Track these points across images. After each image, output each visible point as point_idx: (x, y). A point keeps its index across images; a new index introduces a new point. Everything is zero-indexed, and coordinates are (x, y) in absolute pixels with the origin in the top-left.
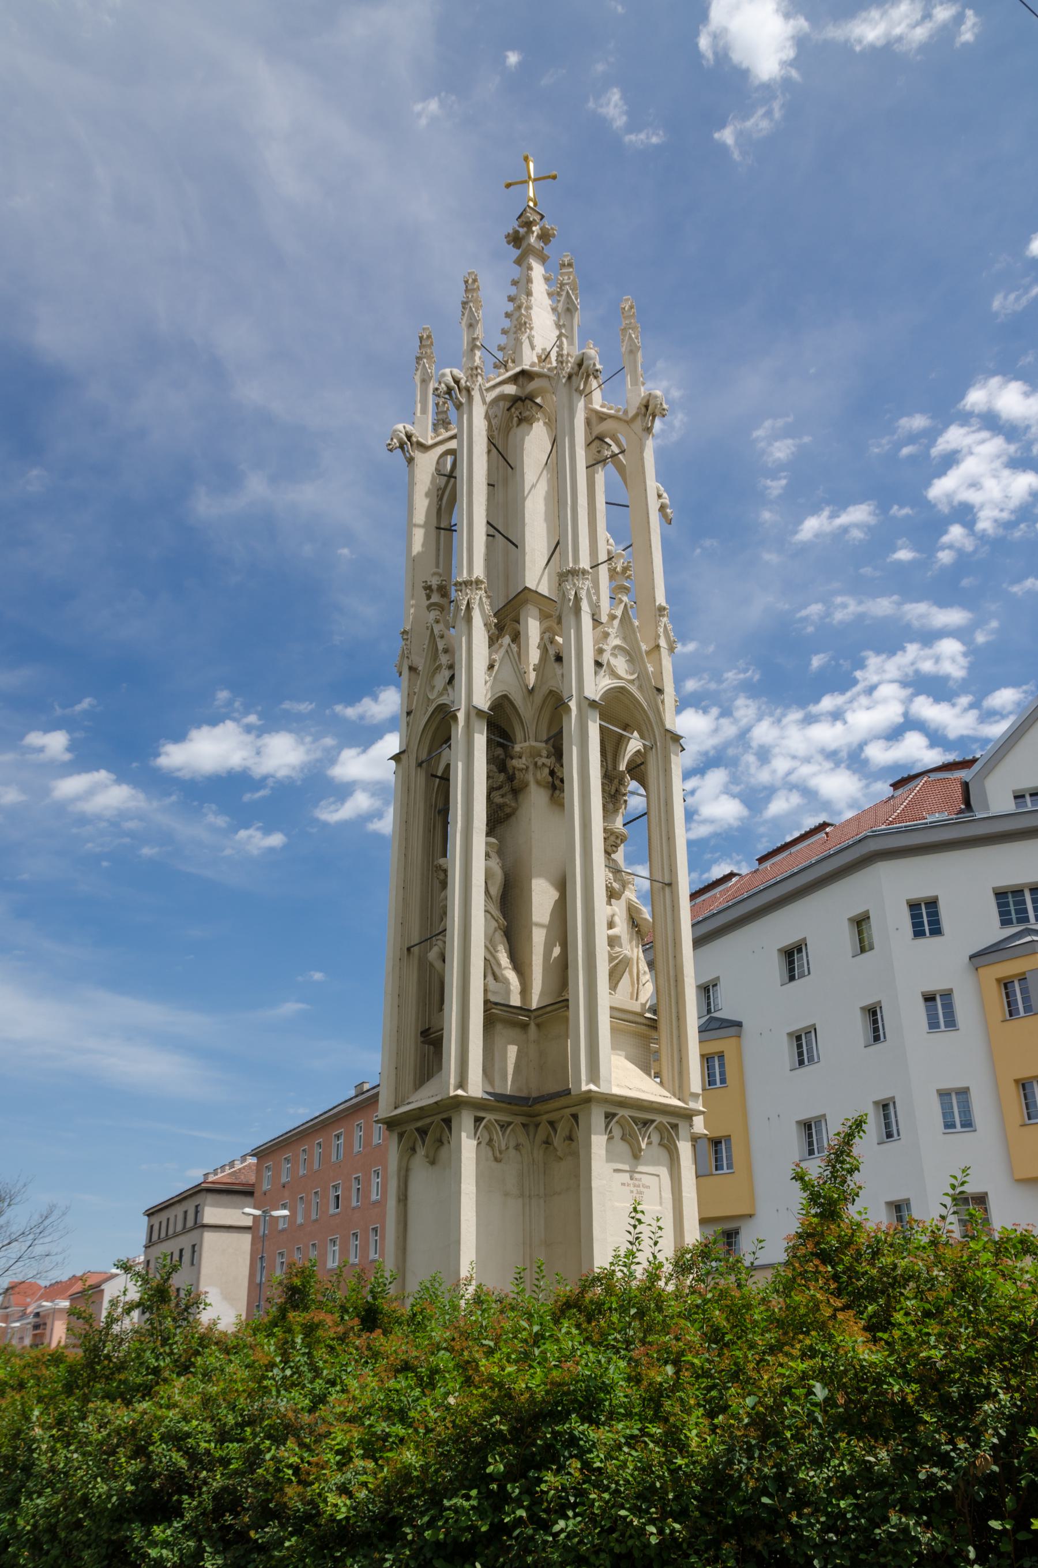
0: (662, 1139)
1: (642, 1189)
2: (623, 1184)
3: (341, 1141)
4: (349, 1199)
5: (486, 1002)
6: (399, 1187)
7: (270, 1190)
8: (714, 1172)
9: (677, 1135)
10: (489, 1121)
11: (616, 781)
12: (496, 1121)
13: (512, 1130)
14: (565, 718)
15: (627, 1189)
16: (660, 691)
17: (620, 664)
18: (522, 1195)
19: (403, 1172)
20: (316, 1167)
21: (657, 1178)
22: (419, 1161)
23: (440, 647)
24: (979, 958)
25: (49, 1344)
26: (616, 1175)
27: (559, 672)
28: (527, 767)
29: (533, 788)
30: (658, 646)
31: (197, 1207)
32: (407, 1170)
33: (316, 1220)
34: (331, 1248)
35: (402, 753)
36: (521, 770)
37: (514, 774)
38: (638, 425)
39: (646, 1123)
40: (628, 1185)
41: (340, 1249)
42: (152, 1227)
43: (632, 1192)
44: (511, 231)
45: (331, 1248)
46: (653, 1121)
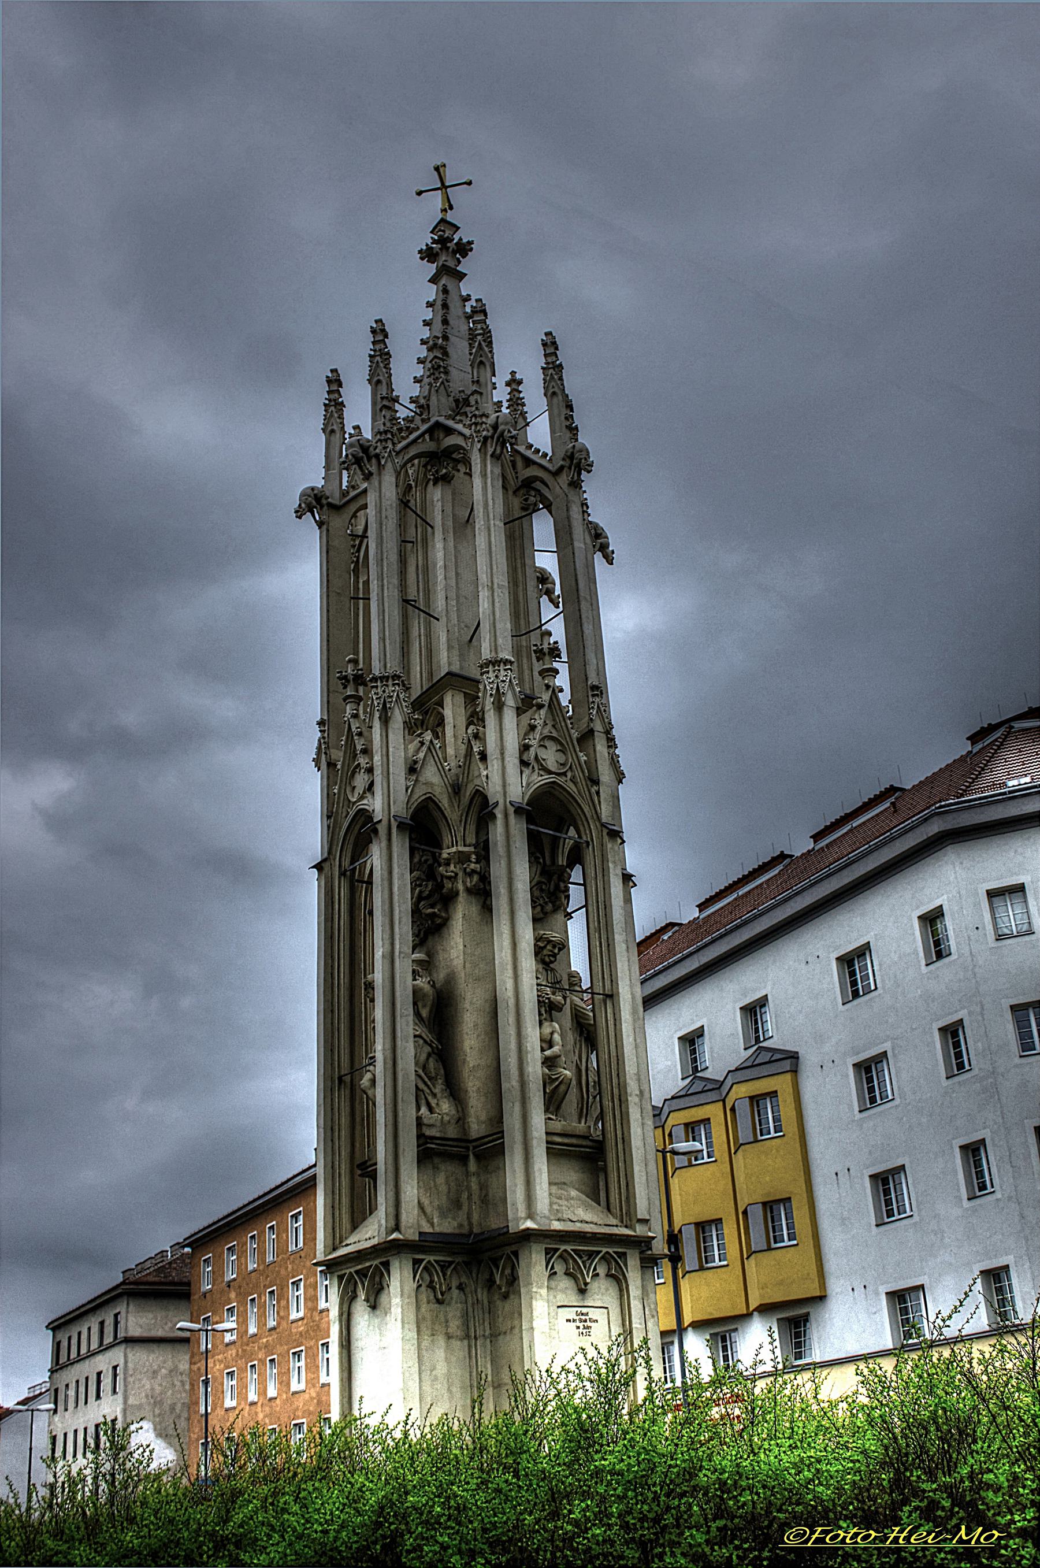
0: (609, 1269)
1: (589, 1324)
2: (568, 1321)
3: (301, 1222)
5: (420, 1136)
7: (211, 1290)
8: (774, 1246)
9: (626, 1265)
10: (429, 1262)
11: (555, 877)
12: (436, 1261)
13: (454, 1269)
14: (491, 827)
15: (573, 1325)
16: (596, 782)
17: (551, 757)
18: (467, 1336)
20: (269, 1258)
21: (605, 1311)
23: (359, 747)
26: (560, 1310)
28: (456, 874)
29: (462, 897)
31: (116, 1316)
32: (349, 1314)
33: (274, 1329)
34: (294, 1364)
35: (324, 861)
36: (449, 878)
38: (564, 479)
39: (591, 1255)
40: (574, 1321)
41: (306, 1365)
42: (59, 1344)
43: (578, 1328)
45: (294, 1364)
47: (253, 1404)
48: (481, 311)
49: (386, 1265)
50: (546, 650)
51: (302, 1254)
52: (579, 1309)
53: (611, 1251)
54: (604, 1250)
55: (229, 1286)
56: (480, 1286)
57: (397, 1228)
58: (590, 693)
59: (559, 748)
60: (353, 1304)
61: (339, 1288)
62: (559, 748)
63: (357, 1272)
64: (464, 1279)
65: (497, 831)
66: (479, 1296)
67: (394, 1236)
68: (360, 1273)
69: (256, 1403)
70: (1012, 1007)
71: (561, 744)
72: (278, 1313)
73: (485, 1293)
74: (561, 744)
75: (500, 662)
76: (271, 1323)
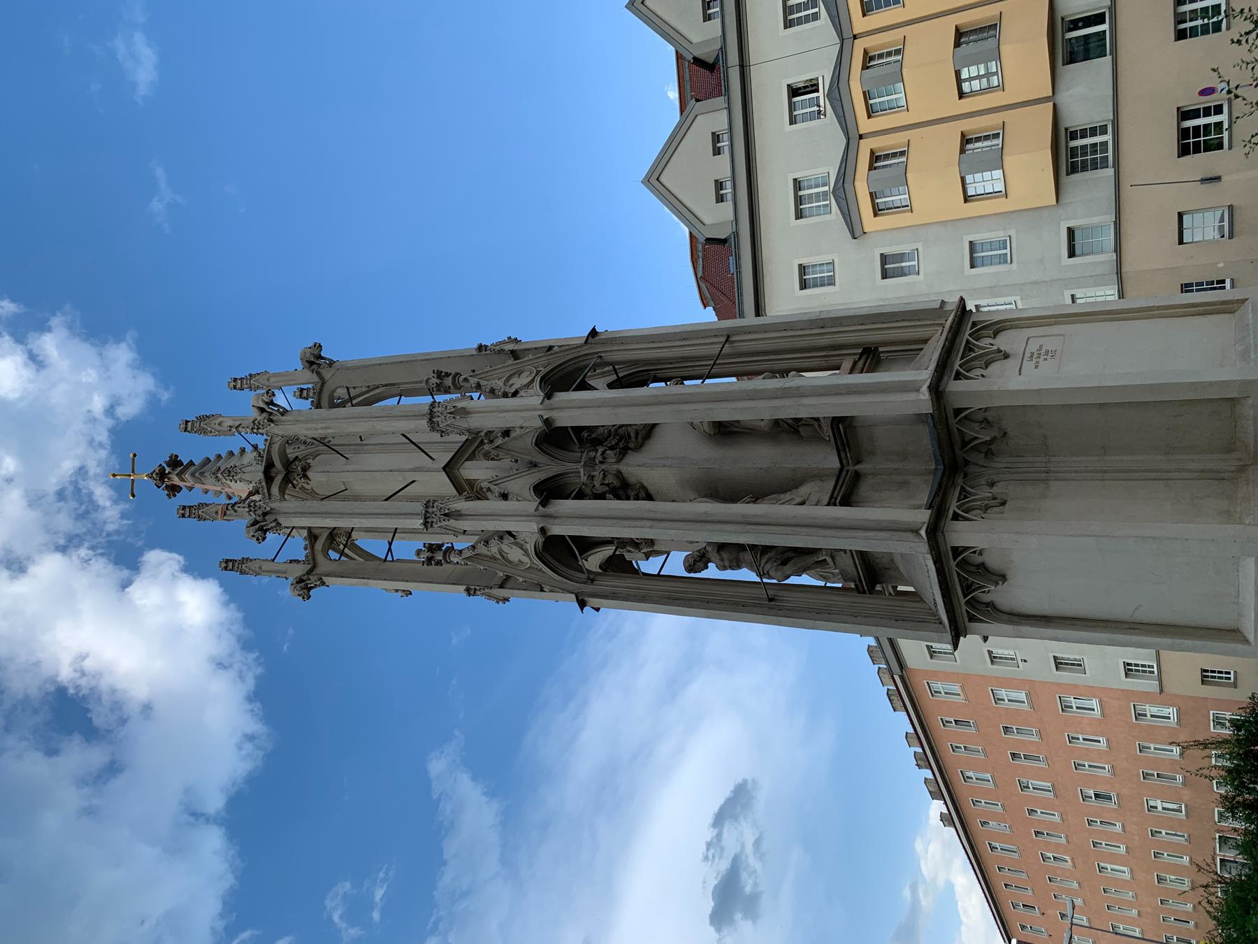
1: (1043, 352)
4: (1058, 845)
6: (1031, 625)
10: (958, 507)
15: (1042, 363)
19: (1015, 619)
21: (1031, 339)
22: (998, 595)
24: (854, 229)
25: (1230, 735)
27: (518, 432)
28: (603, 470)
29: (622, 467)
30: (512, 352)
32: (1012, 614)
36: (605, 476)
37: (608, 485)
38: (327, 374)
41: (1110, 863)
44: (166, 492)
46: (968, 341)
47: (1139, 914)
48: (186, 424)
49: (956, 551)
50: (438, 381)
51: (1021, 848)
52: (1026, 358)
53: (968, 332)
54: (967, 336)
55: (1043, 914)
56: (993, 465)
57: (916, 532)
58: (484, 352)
59: (517, 376)
60: (1000, 607)
61: (981, 621)
62: (517, 376)
63: (965, 596)
64: (983, 481)
65: (566, 419)
66: (1001, 465)
67: (923, 532)
68: (967, 589)
69: (1139, 912)
70: (883, 278)
71: (514, 374)
72: (1067, 878)
73: (999, 460)
74: (514, 374)
75: (431, 411)
76: (1075, 885)
